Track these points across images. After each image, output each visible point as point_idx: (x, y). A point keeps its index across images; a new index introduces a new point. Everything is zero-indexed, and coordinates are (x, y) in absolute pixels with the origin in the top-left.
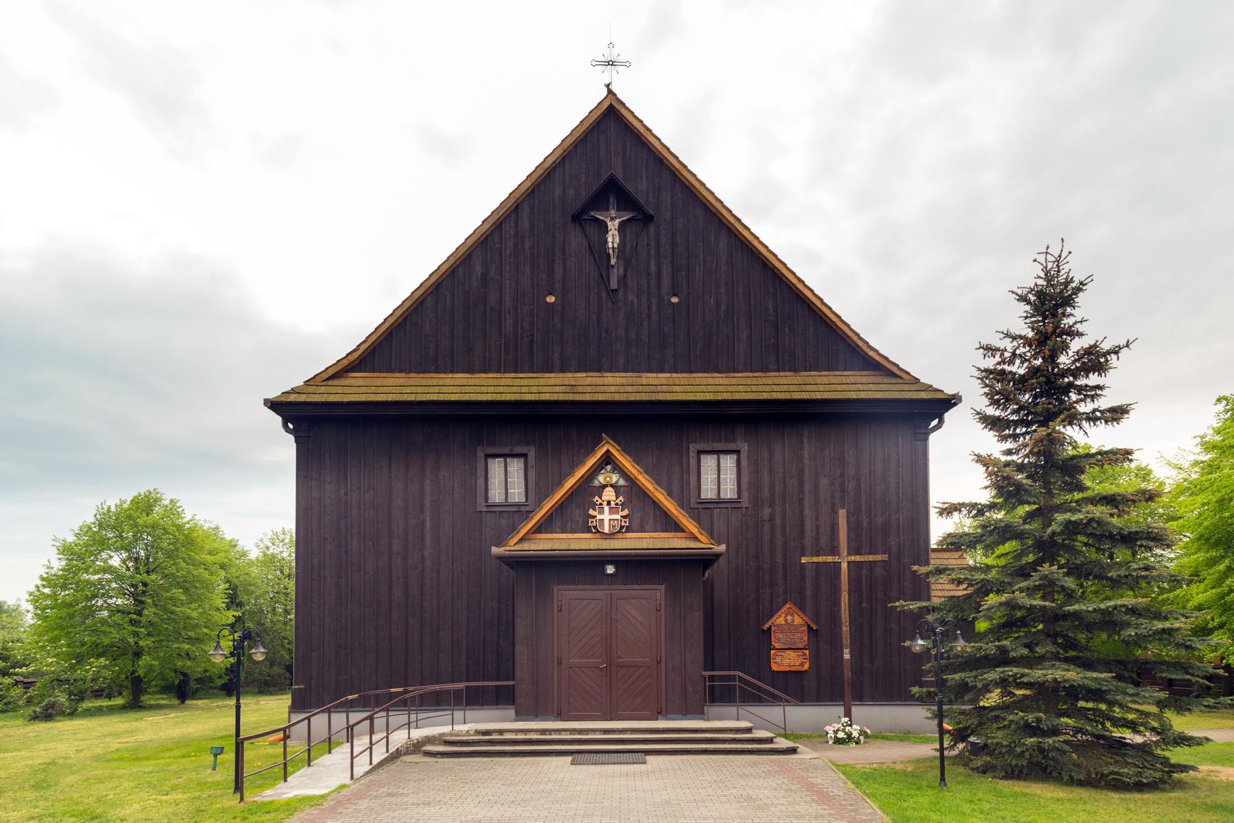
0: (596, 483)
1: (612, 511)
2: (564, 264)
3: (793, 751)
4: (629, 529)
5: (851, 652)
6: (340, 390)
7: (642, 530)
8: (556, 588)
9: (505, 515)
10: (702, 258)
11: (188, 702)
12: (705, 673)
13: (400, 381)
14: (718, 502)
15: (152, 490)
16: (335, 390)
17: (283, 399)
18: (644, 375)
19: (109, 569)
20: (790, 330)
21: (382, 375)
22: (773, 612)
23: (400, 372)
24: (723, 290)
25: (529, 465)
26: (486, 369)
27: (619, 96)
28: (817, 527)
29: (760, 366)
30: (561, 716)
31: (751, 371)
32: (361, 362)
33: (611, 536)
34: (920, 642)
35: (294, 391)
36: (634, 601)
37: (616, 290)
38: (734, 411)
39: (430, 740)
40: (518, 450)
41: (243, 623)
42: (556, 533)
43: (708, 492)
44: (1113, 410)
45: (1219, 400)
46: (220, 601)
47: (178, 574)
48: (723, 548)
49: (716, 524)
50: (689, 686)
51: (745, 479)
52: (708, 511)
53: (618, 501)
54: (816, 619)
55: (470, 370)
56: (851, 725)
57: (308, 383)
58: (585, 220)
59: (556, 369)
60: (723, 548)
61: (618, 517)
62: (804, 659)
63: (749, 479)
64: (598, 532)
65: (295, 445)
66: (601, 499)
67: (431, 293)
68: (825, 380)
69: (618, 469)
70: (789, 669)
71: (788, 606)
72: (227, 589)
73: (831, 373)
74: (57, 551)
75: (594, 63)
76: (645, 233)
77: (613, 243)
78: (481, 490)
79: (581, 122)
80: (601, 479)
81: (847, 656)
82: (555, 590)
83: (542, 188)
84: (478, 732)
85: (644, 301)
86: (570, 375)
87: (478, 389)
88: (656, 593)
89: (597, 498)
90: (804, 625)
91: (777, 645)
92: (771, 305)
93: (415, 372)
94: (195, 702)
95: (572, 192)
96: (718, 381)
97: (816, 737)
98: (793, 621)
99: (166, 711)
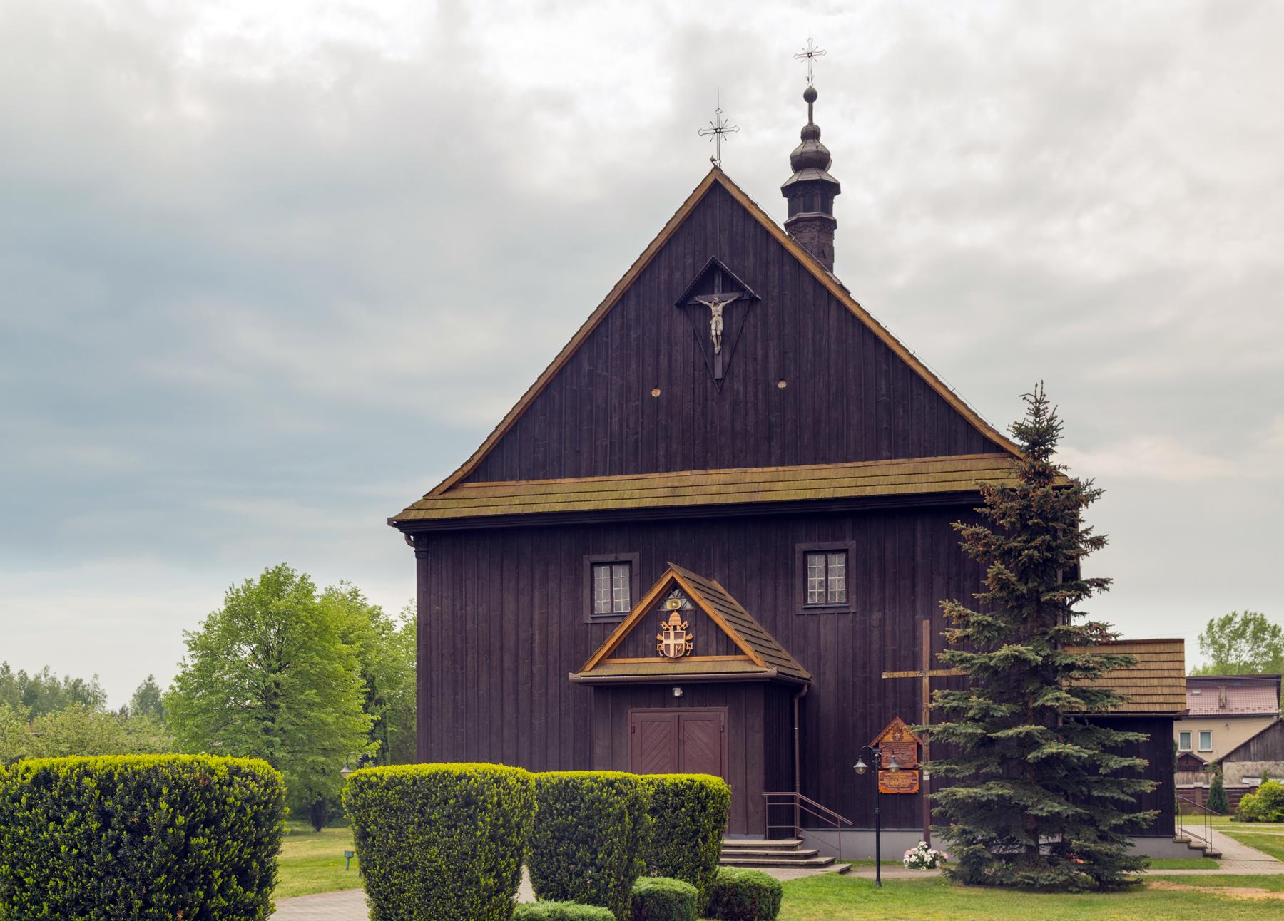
1: (677, 636)
4: (693, 653)
6: (454, 503)
8: (630, 710)
11: (324, 830)
13: (511, 490)
15: (280, 566)
17: (404, 517)
18: (749, 470)
20: (904, 411)
21: (495, 483)
22: (882, 726)
25: (634, 574)
29: (870, 451)
31: (861, 460)
32: (475, 471)
33: (677, 660)
35: (414, 507)
36: (699, 722)
37: (721, 379)
38: (836, 508)
40: (624, 556)
41: (385, 727)
42: (628, 657)
46: (357, 704)
47: (312, 671)
50: (750, 805)
52: (814, 617)
53: (683, 626)
55: (577, 475)
56: (926, 850)
57: (427, 497)
58: (691, 305)
59: (661, 469)
61: (682, 641)
62: (914, 780)
64: (665, 656)
65: (415, 560)
66: (667, 623)
67: (541, 394)
68: (939, 467)
69: (684, 594)
70: (897, 791)
72: (364, 687)
73: (948, 457)
75: (701, 133)
77: (716, 330)
79: (685, 202)
80: (669, 605)
82: (629, 713)
85: (750, 388)
86: (674, 474)
89: (664, 623)
90: (914, 743)
93: (525, 479)
94: (331, 830)
95: (677, 275)
98: (902, 738)
99: (301, 837)
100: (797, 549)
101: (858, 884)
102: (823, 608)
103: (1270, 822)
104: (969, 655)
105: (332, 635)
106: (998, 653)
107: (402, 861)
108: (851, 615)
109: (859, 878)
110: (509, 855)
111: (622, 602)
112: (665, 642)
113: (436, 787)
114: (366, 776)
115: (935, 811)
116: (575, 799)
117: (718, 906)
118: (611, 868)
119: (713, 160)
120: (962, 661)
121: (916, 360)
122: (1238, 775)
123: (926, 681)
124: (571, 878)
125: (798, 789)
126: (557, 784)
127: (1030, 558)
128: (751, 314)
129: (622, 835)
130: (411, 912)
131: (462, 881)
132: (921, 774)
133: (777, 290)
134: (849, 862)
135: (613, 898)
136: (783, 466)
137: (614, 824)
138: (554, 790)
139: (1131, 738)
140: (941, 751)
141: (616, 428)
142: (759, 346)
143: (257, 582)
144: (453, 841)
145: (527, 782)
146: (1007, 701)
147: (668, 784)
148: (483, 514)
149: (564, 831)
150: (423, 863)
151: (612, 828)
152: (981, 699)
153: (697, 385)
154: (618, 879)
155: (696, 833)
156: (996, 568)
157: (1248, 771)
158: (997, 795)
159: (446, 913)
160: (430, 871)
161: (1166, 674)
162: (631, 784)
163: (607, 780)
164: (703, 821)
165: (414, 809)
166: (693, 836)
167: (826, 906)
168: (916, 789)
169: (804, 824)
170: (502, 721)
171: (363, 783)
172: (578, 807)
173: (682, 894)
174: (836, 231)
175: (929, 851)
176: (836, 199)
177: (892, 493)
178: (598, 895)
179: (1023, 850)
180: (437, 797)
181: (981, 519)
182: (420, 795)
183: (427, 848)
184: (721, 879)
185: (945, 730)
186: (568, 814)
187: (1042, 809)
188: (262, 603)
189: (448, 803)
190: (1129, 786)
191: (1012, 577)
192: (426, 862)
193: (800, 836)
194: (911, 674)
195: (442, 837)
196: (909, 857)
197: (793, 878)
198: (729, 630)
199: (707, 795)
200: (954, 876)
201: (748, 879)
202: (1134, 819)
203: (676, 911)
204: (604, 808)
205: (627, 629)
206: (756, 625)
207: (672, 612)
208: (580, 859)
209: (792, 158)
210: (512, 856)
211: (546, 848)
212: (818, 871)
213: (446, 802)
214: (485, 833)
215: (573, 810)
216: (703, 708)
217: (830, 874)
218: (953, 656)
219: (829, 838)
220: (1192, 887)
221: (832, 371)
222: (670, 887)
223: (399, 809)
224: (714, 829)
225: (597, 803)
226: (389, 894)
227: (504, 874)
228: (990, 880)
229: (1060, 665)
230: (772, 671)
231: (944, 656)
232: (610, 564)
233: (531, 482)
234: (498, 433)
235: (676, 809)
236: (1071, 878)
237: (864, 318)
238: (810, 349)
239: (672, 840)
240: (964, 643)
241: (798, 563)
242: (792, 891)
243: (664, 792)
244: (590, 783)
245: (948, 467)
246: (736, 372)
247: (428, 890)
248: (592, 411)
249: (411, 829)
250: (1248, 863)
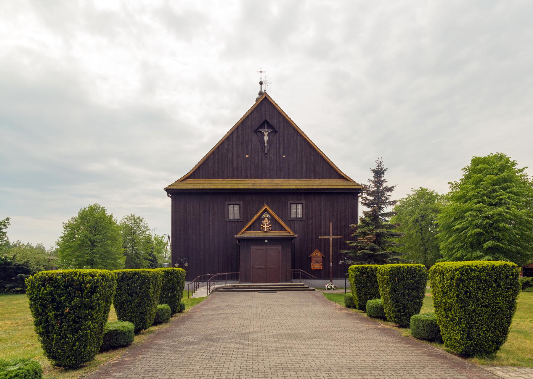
0: (262, 217)
1: (267, 225)
2: (251, 145)
3: (314, 290)
4: (271, 230)
5: (333, 264)
6: (185, 185)
7: (275, 230)
8: (251, 246)
9: (234, 223)
10: (292, 143)
13: (203, 182)
14: (297, 219)
16: (184, 185)
18: (275, 180)
21: (197, 179)
22: (312, 252)
24: (298, 154)
25: (241, 207)
26: (228, 178)
27: (268, 94)
28: (325, 226)
29: (308, 176)
30: (252, 282)
33: (266, 232)
34: (341, 262)
35: (172, 185)
36: (273, 250)
38: (301, 191)
39: (219, 288)
40: (237, 203)
43: (293, 215)
44: (393, 202)
45: (449, 183)
48: (297, 235)
49: (296, 225)
51: (304, 211)
54: (324, 254)
56: (332, 285)
60: (297, 235)
61: (268, 227)
68: (328, 182)
70: (316, 269)
71: (316, 250)
76: (275, 136)
80: (264, 216)
81: (331, 265)
83: (245, 122)
84: (232, 286)
85: (275, 157)
86: (253, 180)
88: (279, 248)
91: (313, 262)
92: (312, 158)
95: (253, 123)
96: (297, 182)
97: (322, 288)
98: (318, 254)
100: (289, 202)
141: (235, 165)
142: (278, 145)
153: (259, 155)
172: (415, 277)
198: (283, 224)
216: (273, 246)
233: (209, 180)
243: (372, 270)
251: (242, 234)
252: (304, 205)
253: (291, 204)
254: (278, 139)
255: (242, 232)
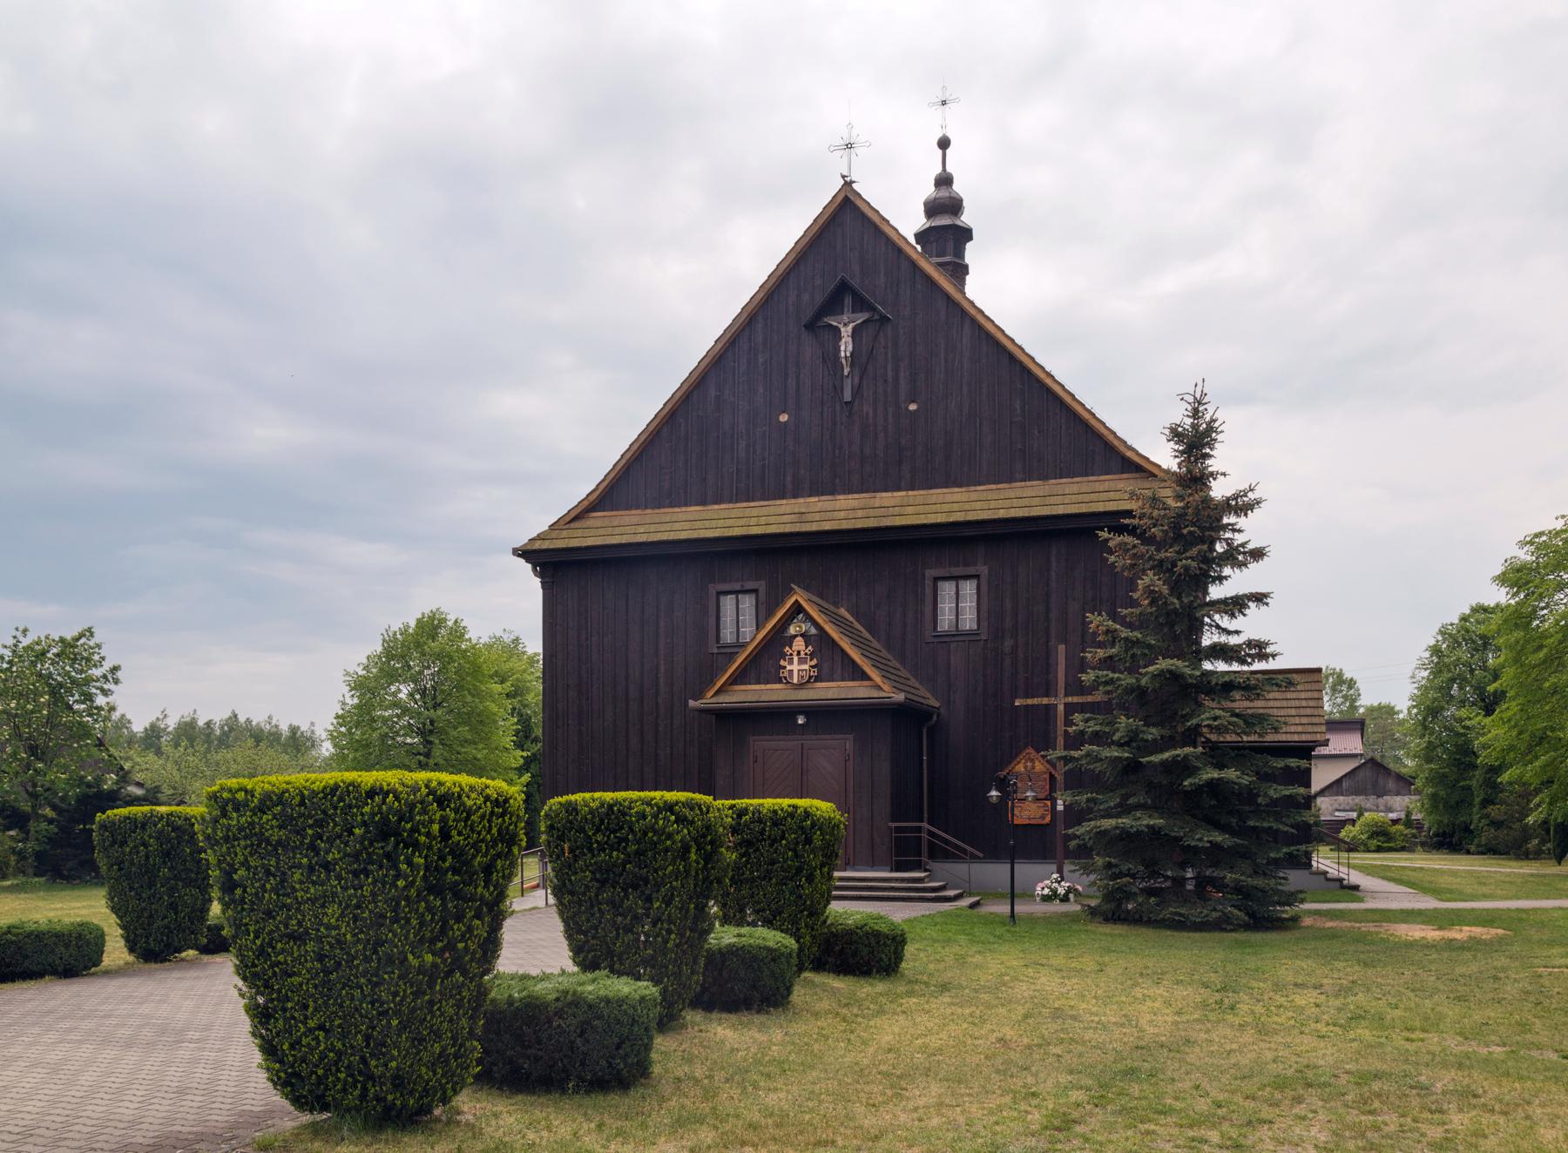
1: (801, 661)
4: (818, 679)
6: (579, 533)
10: (942, 356)
12: (890, 824)
13: (635, 520)
14: (957, 635)
15: (434, 610)
17: (529, 547)
18: (879, 495)
19: (396, 704)
20: (1039, 432)
22: (1012, 756)
23: (636, 509)
26: (718, 500)
29: (1004, 474)
31: (994, 483)
33: (800, 686)
35: (540, 537)
37: (850, 402)
38: (967, 533)
40: (750, 585)
46: (508, 741)
56: (1059, 882)
58: (819, 327)
61: (806, 667)
63: (990, 610)
64: (788, 683)
68: (1075, 488)
69: (809, 618)
70: (1028, 822)
74: (348, 688)
75: (832, 149)
78: (712, 631)
80: (792, 630)
82: (751, 742)
86: (801, 500)
87: (707, 524)
89: (787, 648)
95: (806, 297)
98: (1033, 768)
101: (991, 920)
102: (954, 635)
103: (1369, 851)
104: (1116, 675)
105: (483, 675)
106: (1151, 669)
107: (286, 926)
108: (982, 642)
109: (991, 913)
110: (470, 914)
111: (748, 630)
112: (789, 668)
113: (335, 808)
114: (230, 790)
115: (1073, 843)
116: (622, 828)
117: (829, 955)
118: (670, 922)
119: (843, 177)
120: (1106, 683)
121: (1053, 377)
122: (1330, 809)
123: (1061, 708)
124: (618, 934)
125: (926, 819)
126: (597, 809)
127: (1187, 568)
128: (881, 334)
129: (686, 877)
130: (306, 1007)
131: (379, 959)
132: (1054, 805)
133: (908, 309)
134: (978, 894)
135: (676, 961)
136: (913, 490)
137: (673, 862)
138: (594, 817)
139: (1292, 765)
140: (1076, 779)
142: (890, 367)
143: (413, 624)
144: (362, 895)
145: (506, 801)
146: (1154, 725)
147: (765, 811)
148: (607, 542)
149: (607, 871)
150: (318, 930)
151: (671, 868)
152: (1131, 720)
154: (682, 935)
155: (799, 870)
156: (1149, 579)
157: (1340, 805)
158: (1148, 826)
159: (357, 1009)
160: (329, 943)
161: (1304, 703)
162: (701, 809)
163: (665, 802)
164: (808, 857)
165: (302, 843)
166: (796, 874)
167: (956, 949)
168: (1048, 819)
169: (932, 856)
170: (627, 750)
171: (227, 802)
173: (775, 950)
174: (967, 277)
175: (1063, 883)
176: (969, 245)
177: (1027, 515)
178: (653, 957)
179: (1168, 884)
180: (336, 825)
181: (1132, 531)
182: (310, 822)
183: (323, 906)
184: (832, 924)
185: (1088, 755)
186: (612, 849)
187: (1200, 840)
188: (418, 645)
189: (353, 834)
190: (1288, 816)
191: (1165, 590)
192: (322, 929)
193: (928, 867)
194: (1045, 701)
195: (345, 889)
196: (1041, 889)
197: (920, 914)
198: (855, 655)
199: (813, 825)
200: (1093, 912)
201: (866, 925)
202: (1295, 853)
203: (766, 972)
204: (660, 841)
205: (750, 654)
206: (884, 653)
207: (795, 636)
208: (630, 909)
209: (926, 204)
210: (478, 916)
211: (584, 894)
212: (946, 906)
213: (351, 833)
214: (413, 882)
215: (619, 843)
217: (961, 909)
218: (1097, 677)
219: (960, 869)
220: (1348, 924)
221: (965, 391)
222: (760, 941)
223: (279, 842)
224: (822, 865)
225: (650, 834)
226: (270, 978)
227: (461, 945)
228: (1137, 916)
229: (1217, 684)
230: (900, 697)
231: (1088, 677)
232: (737, 592)
233: (657, 511)
234: (624, 461)
235: (774, 841)
236: (1224, 914)
237: (999, 336)
238: (943, 369)
239: (771, 879)
240: (1108, 663)
241: (928, 591)
242: (918, 930)
243: (760, 821)
244: (642, 807)
245: (1085, 488)
246: (865, 396)
247: (327, 972)
248: (718, 437)
249: (297, 876)
250: (1386, 895)
251: (712, 696)
252: (984, 580)
253: (936, 579)
254: (890, 345)
255: (716, 687)
